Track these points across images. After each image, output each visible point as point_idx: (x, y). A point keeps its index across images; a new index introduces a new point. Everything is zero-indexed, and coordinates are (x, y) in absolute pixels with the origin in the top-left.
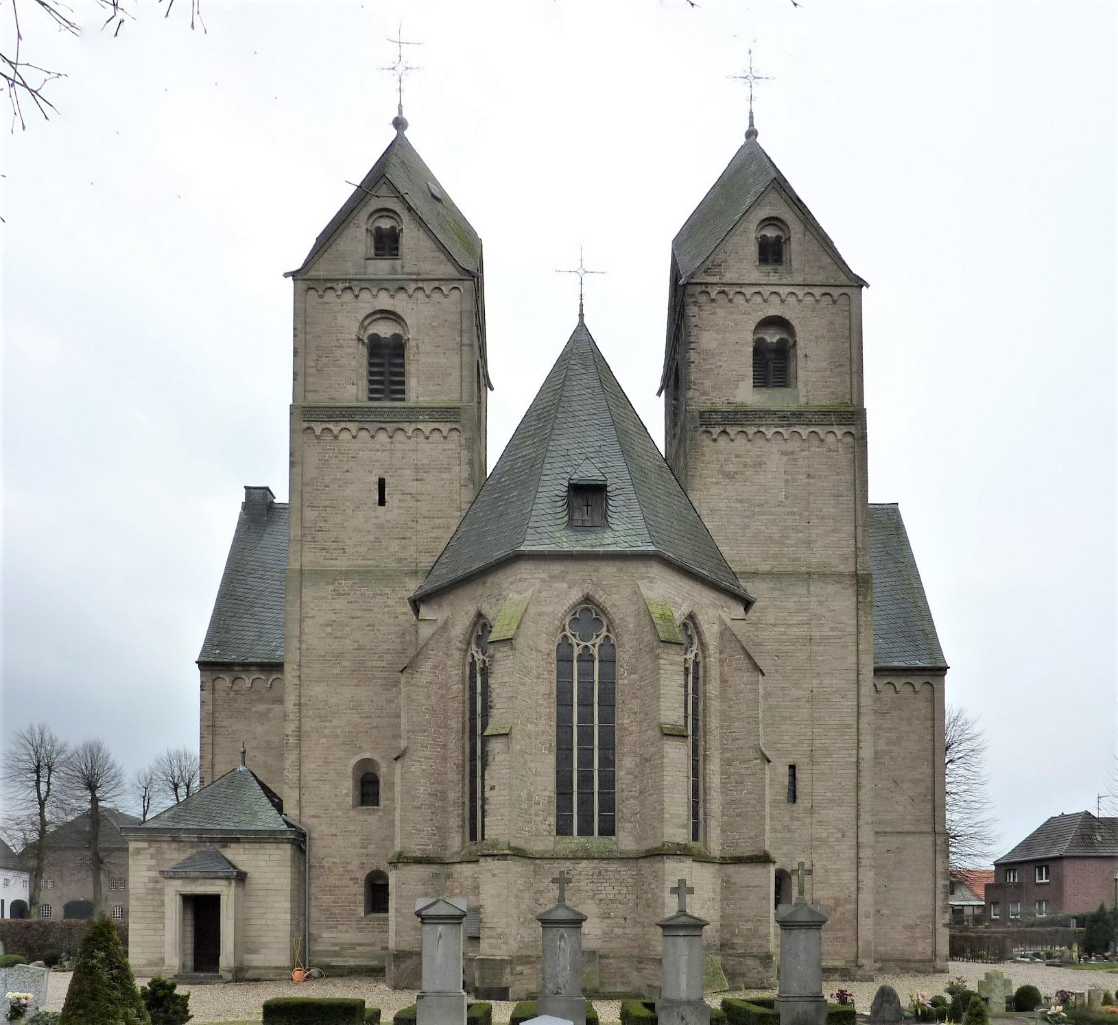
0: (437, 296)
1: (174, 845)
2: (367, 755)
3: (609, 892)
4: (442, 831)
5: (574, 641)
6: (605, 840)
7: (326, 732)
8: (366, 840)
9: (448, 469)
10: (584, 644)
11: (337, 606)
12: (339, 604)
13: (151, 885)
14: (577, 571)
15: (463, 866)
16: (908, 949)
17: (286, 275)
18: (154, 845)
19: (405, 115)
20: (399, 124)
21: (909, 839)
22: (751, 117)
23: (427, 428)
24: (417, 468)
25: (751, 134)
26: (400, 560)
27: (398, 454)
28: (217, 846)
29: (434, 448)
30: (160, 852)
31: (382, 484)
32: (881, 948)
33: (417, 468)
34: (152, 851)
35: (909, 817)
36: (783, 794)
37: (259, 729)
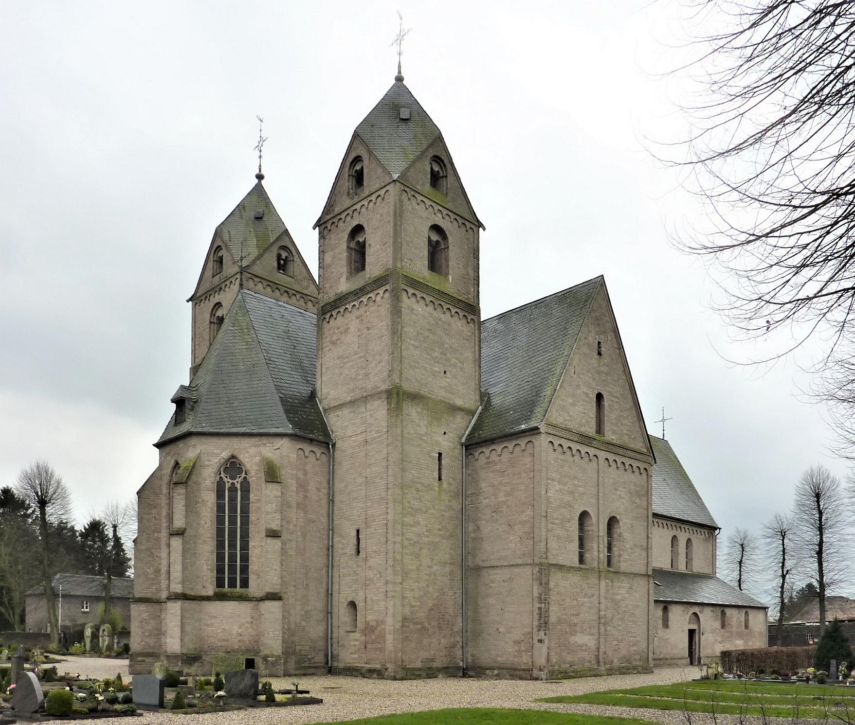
5: (225, 480)
10: (231, 481)
16: (516, 660)
17: (188, 301)
19: (263, 172)
20: (260, 177)
21: (516, 570)
22: (399, 67)
25: (399, 79)
32: (499, 659)
35: (518, 553)
36: (354, 551)
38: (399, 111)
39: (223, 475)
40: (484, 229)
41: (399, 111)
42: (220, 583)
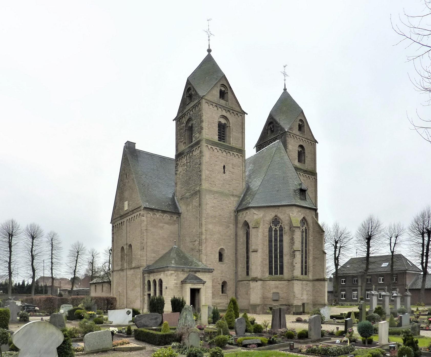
0: (237, 116)
1: (182, 272)
2: (222, 247)
3: (308, 289)
4: (263, 272)
5: (273, 227)
6: (281, 276)
7: (212, 239)
8: (222, 272)
9: (240, 167)
11: (214, 202)
12: (215, 201)
13: (175, 285)
14: (303, 210)
15: (271, 281)
17: (173, 120)
18: (176, 272)
20: (209, 51)
23: (235, 153)
24: (233, 164)
25: (285, 90)
26: (229, 191)
27: (228, 159)
28: (193, 273)
29: (234, 159)
30: (178, 274)
31: (224, 167)
33: (233, 164)
34: (176, 274)
37: (161, 232)
38: (208, 70)
39: (271, 225)
40: (247, 114)
41: (208, 70)
42: (271, 273)
